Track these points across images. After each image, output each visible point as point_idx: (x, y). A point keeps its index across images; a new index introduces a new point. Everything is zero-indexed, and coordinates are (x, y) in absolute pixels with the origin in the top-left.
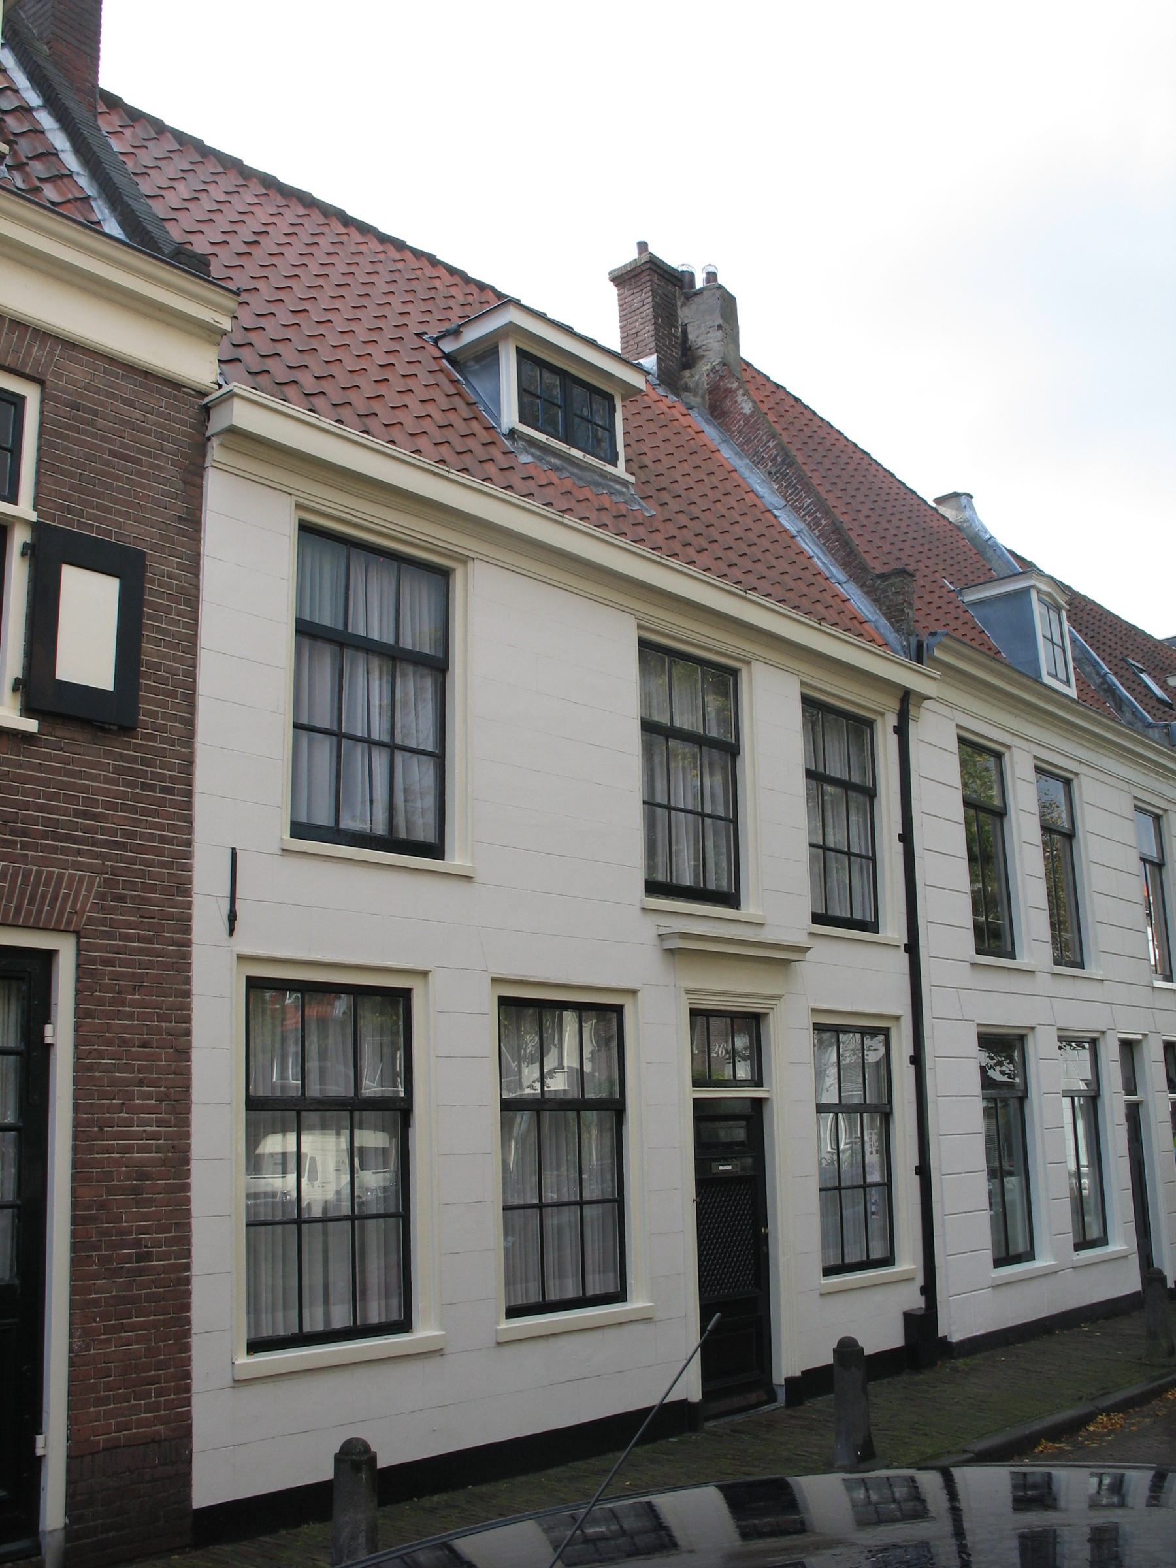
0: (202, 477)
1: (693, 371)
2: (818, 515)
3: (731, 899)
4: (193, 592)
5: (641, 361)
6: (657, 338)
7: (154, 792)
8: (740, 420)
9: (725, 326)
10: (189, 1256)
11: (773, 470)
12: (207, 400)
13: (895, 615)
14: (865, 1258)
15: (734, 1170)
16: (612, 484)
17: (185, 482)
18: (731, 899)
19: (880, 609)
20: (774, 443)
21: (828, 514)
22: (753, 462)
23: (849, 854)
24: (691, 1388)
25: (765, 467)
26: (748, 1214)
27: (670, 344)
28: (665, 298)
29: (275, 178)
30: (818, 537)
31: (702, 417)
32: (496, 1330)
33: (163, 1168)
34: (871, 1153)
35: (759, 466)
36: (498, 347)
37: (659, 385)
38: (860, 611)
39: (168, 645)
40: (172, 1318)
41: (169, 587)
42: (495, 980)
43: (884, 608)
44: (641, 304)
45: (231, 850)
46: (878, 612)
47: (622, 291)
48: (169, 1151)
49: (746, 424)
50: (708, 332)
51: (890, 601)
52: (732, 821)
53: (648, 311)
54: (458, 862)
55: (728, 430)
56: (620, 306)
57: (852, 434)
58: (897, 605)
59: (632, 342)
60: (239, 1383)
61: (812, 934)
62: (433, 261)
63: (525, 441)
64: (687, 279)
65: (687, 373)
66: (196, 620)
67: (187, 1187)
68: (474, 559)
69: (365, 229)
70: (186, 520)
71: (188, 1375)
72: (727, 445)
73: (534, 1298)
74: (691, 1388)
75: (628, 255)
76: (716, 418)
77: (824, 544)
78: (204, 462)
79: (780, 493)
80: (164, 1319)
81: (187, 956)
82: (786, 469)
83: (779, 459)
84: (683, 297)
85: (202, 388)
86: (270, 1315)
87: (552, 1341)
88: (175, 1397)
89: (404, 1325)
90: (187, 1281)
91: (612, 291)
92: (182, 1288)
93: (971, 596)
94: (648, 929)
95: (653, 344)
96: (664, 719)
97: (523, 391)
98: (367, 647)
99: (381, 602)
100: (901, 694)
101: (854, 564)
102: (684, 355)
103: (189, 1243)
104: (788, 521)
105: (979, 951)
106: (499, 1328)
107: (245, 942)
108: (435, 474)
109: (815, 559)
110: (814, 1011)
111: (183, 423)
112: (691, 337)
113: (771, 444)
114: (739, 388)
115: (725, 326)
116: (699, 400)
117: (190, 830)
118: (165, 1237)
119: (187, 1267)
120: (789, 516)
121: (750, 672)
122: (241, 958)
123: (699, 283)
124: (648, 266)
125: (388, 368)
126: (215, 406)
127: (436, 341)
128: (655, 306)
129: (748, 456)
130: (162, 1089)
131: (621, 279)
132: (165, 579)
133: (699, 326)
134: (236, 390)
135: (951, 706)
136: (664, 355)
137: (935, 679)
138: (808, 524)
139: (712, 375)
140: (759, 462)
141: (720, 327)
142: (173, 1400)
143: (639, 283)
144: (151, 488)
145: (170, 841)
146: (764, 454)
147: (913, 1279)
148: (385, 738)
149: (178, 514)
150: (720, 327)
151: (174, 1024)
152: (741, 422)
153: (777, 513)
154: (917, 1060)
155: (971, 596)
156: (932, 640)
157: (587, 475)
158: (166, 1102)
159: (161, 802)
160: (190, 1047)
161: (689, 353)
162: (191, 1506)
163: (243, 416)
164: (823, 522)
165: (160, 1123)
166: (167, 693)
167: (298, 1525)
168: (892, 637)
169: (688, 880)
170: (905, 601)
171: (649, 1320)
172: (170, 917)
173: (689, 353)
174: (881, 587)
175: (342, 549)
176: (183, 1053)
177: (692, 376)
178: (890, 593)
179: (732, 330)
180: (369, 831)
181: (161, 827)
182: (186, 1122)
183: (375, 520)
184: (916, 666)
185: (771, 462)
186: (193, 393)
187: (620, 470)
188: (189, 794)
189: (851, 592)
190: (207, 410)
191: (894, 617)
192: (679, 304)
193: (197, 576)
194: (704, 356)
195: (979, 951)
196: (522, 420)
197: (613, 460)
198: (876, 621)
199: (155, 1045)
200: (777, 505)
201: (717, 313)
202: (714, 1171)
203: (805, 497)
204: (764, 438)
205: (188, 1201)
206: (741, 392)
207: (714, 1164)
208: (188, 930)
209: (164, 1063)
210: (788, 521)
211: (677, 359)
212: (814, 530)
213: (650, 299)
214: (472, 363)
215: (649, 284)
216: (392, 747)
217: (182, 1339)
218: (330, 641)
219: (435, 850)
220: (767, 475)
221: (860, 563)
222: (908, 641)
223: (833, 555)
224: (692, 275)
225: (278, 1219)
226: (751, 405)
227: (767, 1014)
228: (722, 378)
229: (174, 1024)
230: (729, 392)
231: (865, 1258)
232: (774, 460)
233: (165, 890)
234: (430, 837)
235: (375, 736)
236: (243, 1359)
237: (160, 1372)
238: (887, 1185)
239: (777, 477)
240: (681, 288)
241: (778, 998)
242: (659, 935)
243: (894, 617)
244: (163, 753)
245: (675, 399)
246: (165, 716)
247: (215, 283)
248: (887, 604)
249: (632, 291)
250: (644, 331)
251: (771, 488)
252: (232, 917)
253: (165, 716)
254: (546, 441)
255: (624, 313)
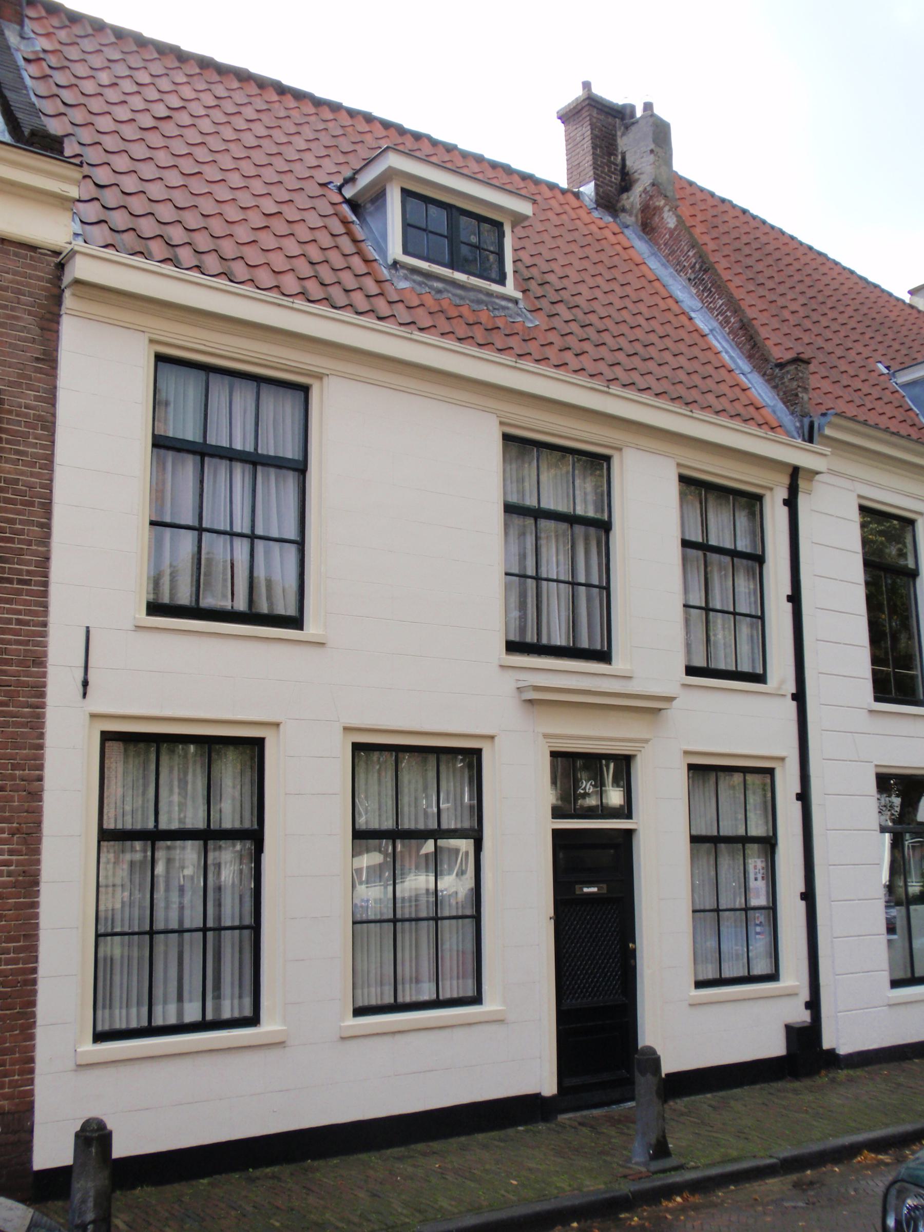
0: (58, 323)
1: (630, 193)
2: (728, 314)
3: (604, 656)
4: (50, 418)
5: (581, 189)
6: (595, 166)
7: (10, 584)
8: (666, 234)
9: (657, 150)
10: (36, 961)
11: (692, 277)
12: (61, 257)
13: (790, 399)
14: (746, 974)
15: (600, 892)
16: (497, 301)
17: (42, 329)
18: (604, 656)
19: (778, 395)
20: (694, 251)
21: (736, 312)
22: (676, 271)
23: (734, 614)
24: (548, 1086)
25: (686, 274)
26: (614, 931)
27: (609, 171)
28: (604, 129)
29: (212, 59)
30: (728, 334)
31: (636, 234)
32: (340, 1027)
33: (14, 889)
34: (756, 879)
35: (681, 274)
36: (385, 190)
37: (596, 209)
38: (759, 398)
39: (25, 464)
40: (18, 1012)
41: (26, 415)
42: (347, 729)
43: (781, 393)
44: (582, 137)
45: (85, 629)
46: (776, 397)
47: (568, 127)
48: (19, 875)
49: (671, 237)
50: (642, 157)
51: (786, 387)
52: (606, 588)
53: (587, 144)
54: (312, 632)
55: (657, 244)
56: (566, 141)
57: (806, 236)
58: (792, 390)
59: (575, 173)
60: (80, 1067)
61: (685, 686)
62: (369, 118)
63: (408, 269)
64: (628, 111)
65: (625, 196)
66: (53, 442)
67: (35, 905)
68: (328, 375)
69: (300, 96)
70: (43, 359)
71: (32, 1060)
72: (656, 257)
73: (389, 999)
74: (548, 1086)
75: (573, 94)
76: (647, 234)
77: (733, 340)
78: (60, 310)
79: (698, 296)
80: (11, 1014)
81: (41, 716)
82: (703, 275)
83: (697, 266)
84: (622, 128)
85: (57, 249)
86: (124, 1011)
87: (398, 1037)
88: (19, 1078)
89: (253, 1020)
90: (34, 982)
91: (560, 127)
92: (29, 988)
93: (905, 377)
94: (508, 683)
95: (591, 173)
96: (530, 501)
97: (407, 226)
98: (230, 455)
99: (244, 418)
100: (790, 470)
101: (757, 356)
102: (623, 179)
103: (36, 951)
104: (703, 322)
105: (877, 699)
106: (342, 1024)
107: (99, 702)
108: (279, 305)
109: (724, 354)
110: (686, 753)
111: (40, 279)
112: (629, 163)
113: (691, 254)
114: (666, 205)
115: (657, 150)
116: (633, 219)
117: (46, 613)
118: (14, 946)
119: (34, 970)
120: (704, 317)
121: (621, 457)
122: (93, 716)
123: (639, 113)
124: (587, 102)
125: (276, 216)
126: (68, 261)
127: (340, 189)
128: (594, 138)
129: (672, 266)
130: (15, 825)
131: (568, 116)
132: (23, 409)
133: (635, 152)
134: (76, 248)
135: (852, 479)
136: (602, 182)
137: (825, 455)
138: (720, 323)
139: (643, 196)
140: (681, 270)
141: (652, 151)
142: (17, 1080)
143: (581, 119)
144: (8, 335)
145: (27, 623)
146: (685, 264)
147: (796, 994)
148: (247, 531)
149: (35, 355)
150: (652, 151)
151: (27, 772)
152: (667, 236)
153: (693, 315)
154: (804, 797)
155: (905, 377)
156: (823, 420)
157: (472, 295)
158: (18, 836)
159: (19, 592)
160: (42, 790)
161: (627, 178)
162: (32, 1167)
163: (81, 269)
164: (732, 320)
165: (11, 852)
166: (24, 503)
167: (133, 1187)
168: (787, 419)
169: (559, 639)
170: (799, 386)
171: (501, 1021)
172: (26, 685)
173: (627, 178)
174: (779, 375)
175: (202, 374)
176: (36, 796)
177: (628, 198)
178: (786, 380)
179: (665, 153)
180: (230, 608)
181: (19, 612)
182: (37, 851)
183: (231, 349)
184: (808, 445)
185: (691, 269)
186: (49, 253)
187: (510, 288)
188: (46, 584)
189: (753, 381)
190: (61, 266)
191: (789, 401)
192: (619, 133)
193: (54, 405)
194: (639, 179)
195: (877, 699)
196: (406, 252)
197: (502, 281)
198: (774, 406)
199: (8, 789)
200: (694, 308)
201: (651, 139)
202: (577, 892)
203: (718, 299)
204: (686, 248)
205: (36, 916)
206: (667, 208)
207: (577, 887)
208: (43, 695)
209: (16, 804)
210: (703, 322)
211: (616, 184)
212: (725, 327)
213: (589, 132)
214: (369, 205)
215: (588, 118)
216: (252, 537)
217: (28, 1029)
218: (194, 452)
219: (296, 622)
220: (687, 281)
221: (763, 354)
222: (801, 422)
223: (740, 349)
224: (633, 108)
225: (136, 929)
226: (675, 219)
227: (634, 756)
228: (651, 197)
229: (27, 772)
230: (658, 210)
231: (746, 974)
232: (693, 267)
233: (20, 663)
234: (292, 611)
235: (237, 529)
236: (88, 1047)
237: (5, 1057)
238: (772, 909)
239: (695, 283)
240: (623, 119)
241: (646, 741)
242: (518, 688)
243: (789, 401)
244: (21, 552)
245: (611, 219)
246: (22, 522)
247: (66, 161)
248: (784, 389)
249: (575, 127)
250: (584, 162)
251: (690, 293)
252: (85, 684)
253: (22, 522)
254: (429, 268)
255: (569, 147)
